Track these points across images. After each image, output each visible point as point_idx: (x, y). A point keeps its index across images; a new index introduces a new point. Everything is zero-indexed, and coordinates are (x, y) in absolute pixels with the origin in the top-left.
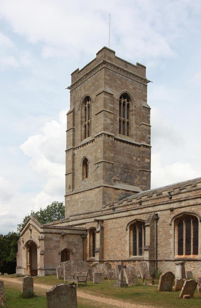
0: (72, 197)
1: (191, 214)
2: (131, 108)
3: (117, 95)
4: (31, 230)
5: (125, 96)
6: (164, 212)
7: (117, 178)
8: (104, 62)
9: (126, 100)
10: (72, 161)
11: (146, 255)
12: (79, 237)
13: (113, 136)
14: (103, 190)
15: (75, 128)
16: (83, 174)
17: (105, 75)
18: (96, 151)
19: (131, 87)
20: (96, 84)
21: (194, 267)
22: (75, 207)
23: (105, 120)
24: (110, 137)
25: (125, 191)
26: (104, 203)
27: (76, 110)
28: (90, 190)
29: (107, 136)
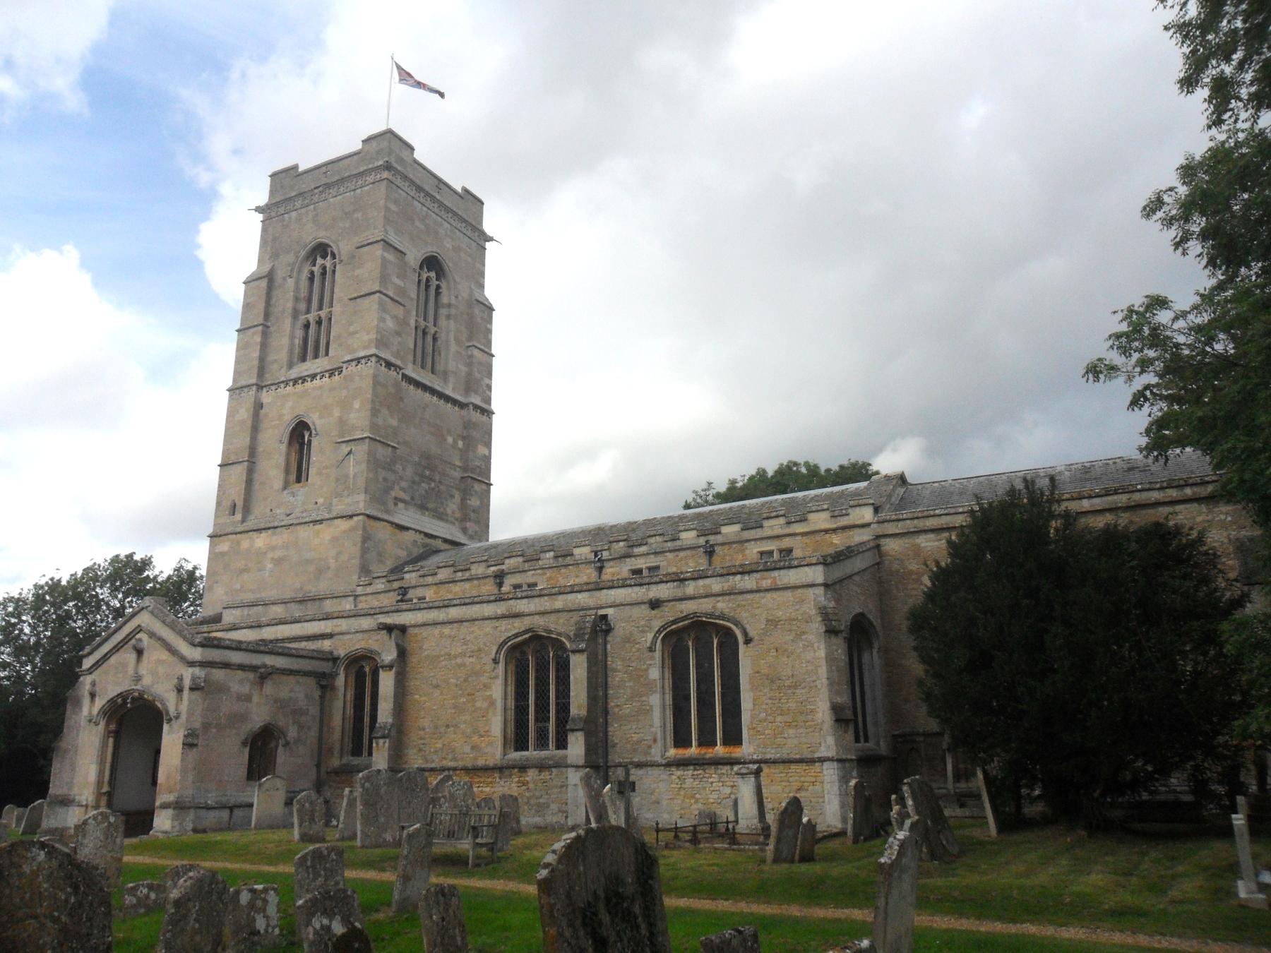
0: (238, 543)
1: (717, 621)
2: (444, 299)
3: (414, 257)
4: (140, 652)
5: (432, 263)
6: (627, 611)
7: (402, 495)
8: (388, 167)
9: (433, 274)
10: (249, 423)
11: (576, 747)
12: (311, 681)
13: (401, 369)
14: (364, 529)
15: (269, 324)
16: (287, 471)
17: (387, 198)
18: (345, 404)
19: (448, 244)
20: (356, 215)
21: (732, 784)
22: (245, 576)
23: (382, 320)
24: (392, 368)
25: (422, 536)
26: (365, 570)
27: (280, 274)
28: (315, 522)
29: (384, 365)
